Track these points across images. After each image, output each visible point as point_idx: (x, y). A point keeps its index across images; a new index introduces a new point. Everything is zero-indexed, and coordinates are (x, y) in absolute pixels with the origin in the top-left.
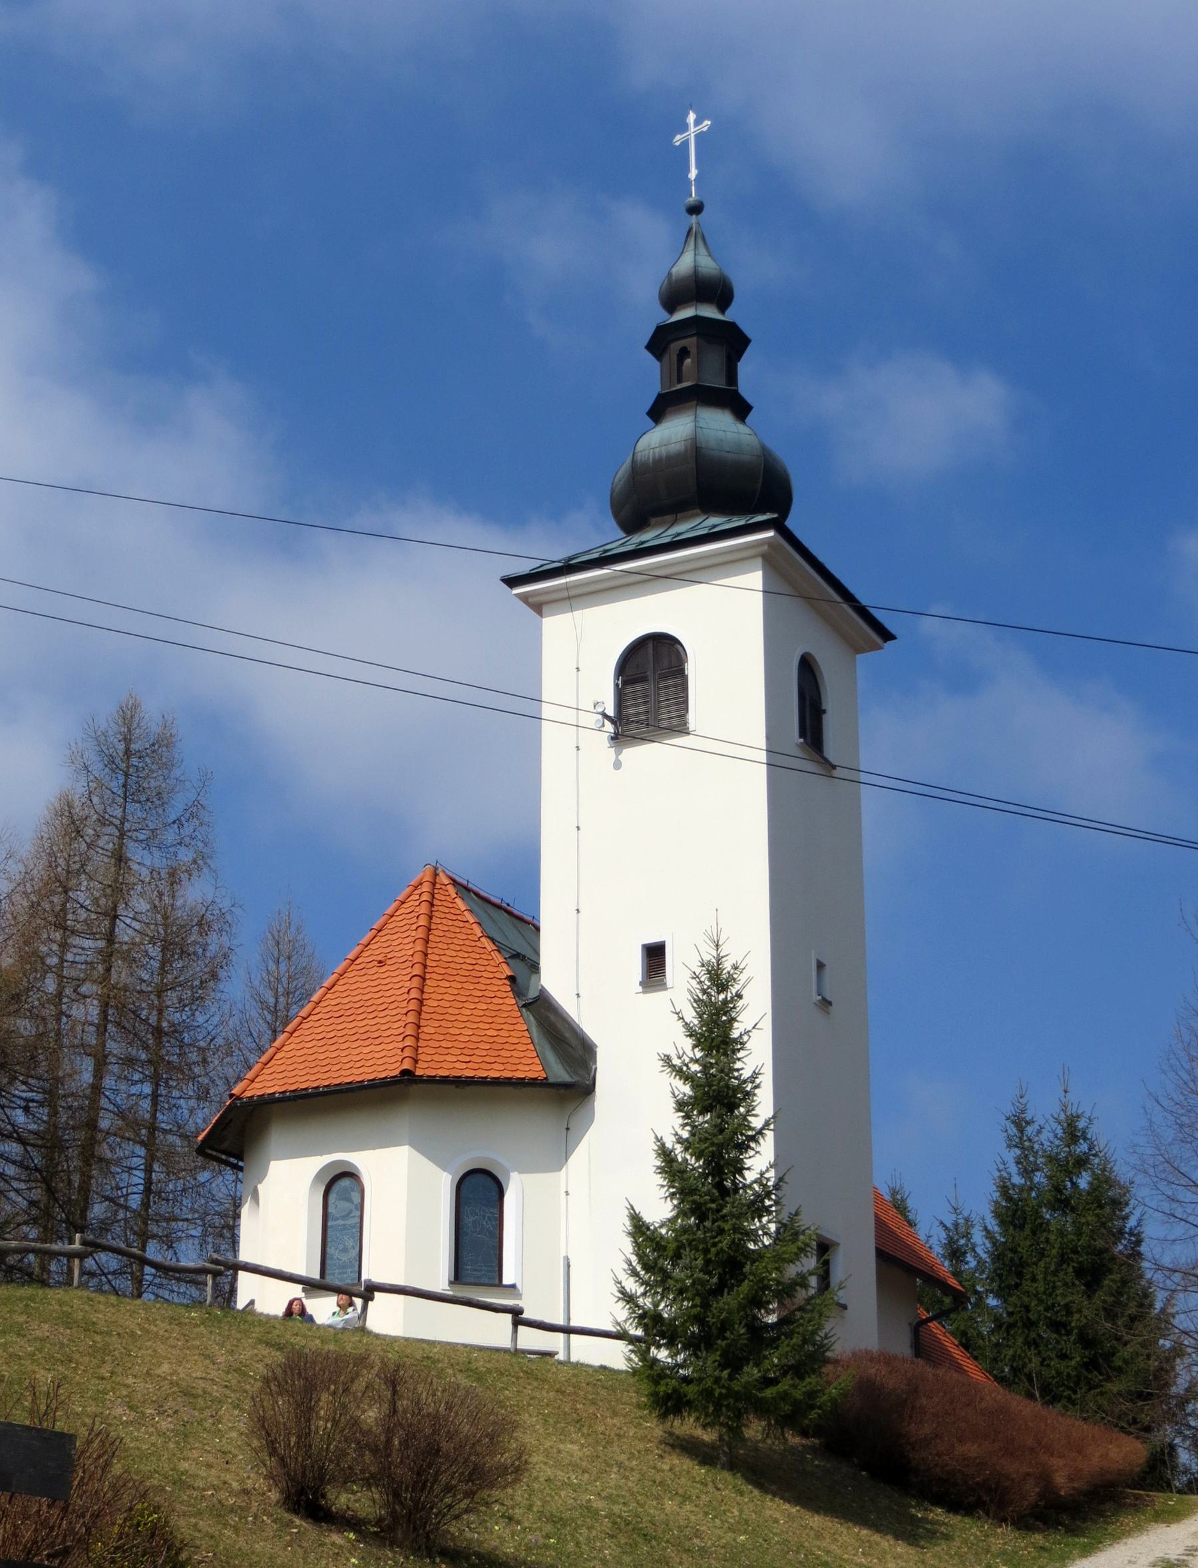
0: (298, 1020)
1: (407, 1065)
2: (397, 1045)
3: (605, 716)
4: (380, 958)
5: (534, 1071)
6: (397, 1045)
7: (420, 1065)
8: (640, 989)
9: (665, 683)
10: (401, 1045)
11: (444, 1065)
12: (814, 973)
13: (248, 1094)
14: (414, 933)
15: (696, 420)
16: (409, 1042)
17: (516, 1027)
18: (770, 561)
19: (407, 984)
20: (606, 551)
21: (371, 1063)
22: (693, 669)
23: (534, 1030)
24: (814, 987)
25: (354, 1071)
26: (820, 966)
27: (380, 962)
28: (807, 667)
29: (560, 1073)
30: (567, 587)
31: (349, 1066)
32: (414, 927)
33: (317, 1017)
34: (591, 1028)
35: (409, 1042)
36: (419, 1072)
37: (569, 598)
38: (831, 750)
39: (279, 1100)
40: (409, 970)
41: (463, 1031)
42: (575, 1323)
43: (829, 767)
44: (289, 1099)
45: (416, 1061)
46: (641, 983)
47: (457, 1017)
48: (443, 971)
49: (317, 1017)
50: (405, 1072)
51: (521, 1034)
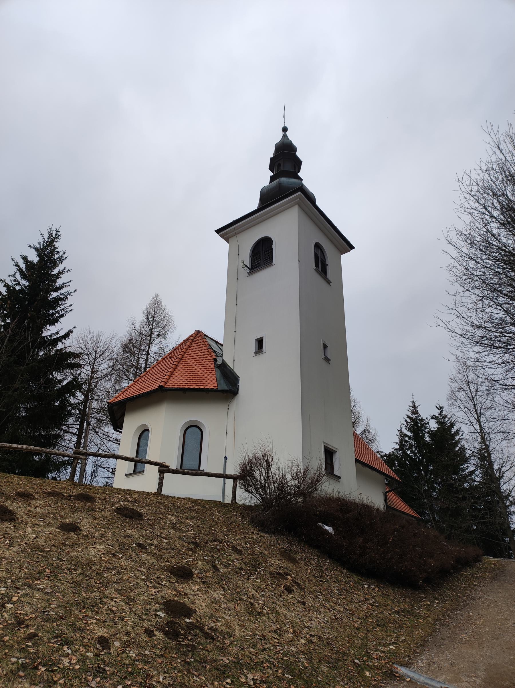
8: (254, 355)
24: (323, 353)
29: (224, 386)
34: (237, 370)
38: (330, 276)
43: (329, 282)
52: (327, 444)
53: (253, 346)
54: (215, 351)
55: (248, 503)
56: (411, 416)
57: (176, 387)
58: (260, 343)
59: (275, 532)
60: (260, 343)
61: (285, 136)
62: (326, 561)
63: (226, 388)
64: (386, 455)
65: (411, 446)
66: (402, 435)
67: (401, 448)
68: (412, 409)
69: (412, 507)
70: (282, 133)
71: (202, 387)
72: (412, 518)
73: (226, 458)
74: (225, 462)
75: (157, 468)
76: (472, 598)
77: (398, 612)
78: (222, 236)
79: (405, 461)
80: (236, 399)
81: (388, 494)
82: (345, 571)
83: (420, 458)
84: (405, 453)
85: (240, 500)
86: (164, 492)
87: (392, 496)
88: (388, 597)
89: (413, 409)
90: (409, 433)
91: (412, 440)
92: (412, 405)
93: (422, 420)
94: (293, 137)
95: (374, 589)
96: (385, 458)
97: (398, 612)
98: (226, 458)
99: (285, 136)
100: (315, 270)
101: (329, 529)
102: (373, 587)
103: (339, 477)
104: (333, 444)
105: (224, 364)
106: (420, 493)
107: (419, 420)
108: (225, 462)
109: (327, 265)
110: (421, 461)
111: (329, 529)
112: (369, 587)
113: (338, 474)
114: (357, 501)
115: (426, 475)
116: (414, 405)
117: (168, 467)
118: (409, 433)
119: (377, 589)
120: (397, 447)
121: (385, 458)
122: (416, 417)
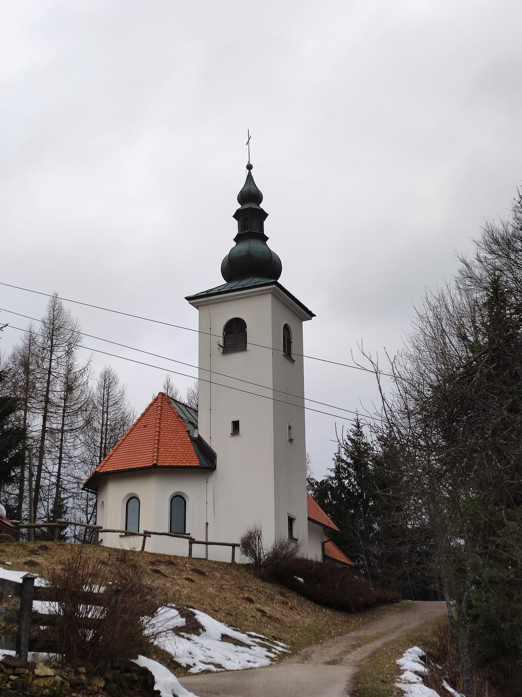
0: (109, 456)
1: (155, 462)
2: (151, 455)
3: (220, 346)
4: (144, 425)
5: (196, 463)
6: (151, 455)
7: (159, 461)
8: (231, 436)
9: (239, 334)
10: (152, 455)
11: (167, 462)
12: (288, 430)
13: (101, 471)
14: (156, 416)
15: (250, 245)
16: (156, 446)
17: (190, 448)
18: (274, 295)
19: (154, 434)
20: (220, 290)
21: (142, 461)
22: (249, 330)
23: (196, 449)
24: (288, 435)
25: (137, 464)
26: (290, 427)
27: (145, 426)
28: (286, 328)
29: (206, 464)
30: (207, 301)
31: (135, 462)
32: (156, 414)
33: (143, 420)
34: (215, 447)
35: (156, 446)
36: (159, 464)
37: (208, 305)
38: (294, 357)
39: (112, 473)
40: (154, 429)
41: (173, 450)
42: (209, 541)
43: (293, 361)
44: (115, 473)
45: (157, 460)
46: (231, 434)
47: (167, 459)
48: (166, 429)
49: (143, 420)
50: (154, 464)
51: (188, 442)
52: (290, 514)
53: (229, 428)
54: (182, 418)
55: (245, 563)
56: (352, 437)
57: (166, 464)
58: (236, 425)
59: (271, 582)
60: (236, 425)
61: (250, 178)
62: (301, 598)
63: (207, 465)
64: (317, 483)
65: (350, 474)
66: (339, 459)
67: (337, 477)
68: (355, 428)
69: (343, 551)
70: (246, 172)
71: (188, 464)
72: (346, 566)
73: (207, 524)
74: (207, 527)
75: (188, 540)
76: (382, 618)
77: (342, 621)
78: (192, 304)
79: (341, 493)
80: (214, 474)
81: (326, 544)
82: (312, 603)
83: (360, 491)
84: (341, 484)
85: (237, 560)
86: (193, 556)
87: (330, 545)
88: (336, 615)
89: (356, 429)
90: (349, 460)
91: (352, 468)
92: (355, 424)
93: (366, 444)
94: (260, 184)
95: (328, 612)
96: (316, 487)
97: (342, 621)
98: (207, 524)
99: (250, 178)
100: (284, 355)
101: (300, 579)
102: (328, 610)
103: (297, 540)
104: (294, 514)
105: (200, 439)
106: (355, 534)
107: (363, 444)
108: (207, 527)
109: (292, 342)
110: (361, 495)
111: (300, 579)
112: (326, 611)
113: (296, 538)
114: (314, 560)
115: (365, 512)
116: (359, 425)
117: (194, 539)
118: (349, 460)
119: (330, 612)
120: (333, 475)
121: (316, 487)
122: (359, 439)
